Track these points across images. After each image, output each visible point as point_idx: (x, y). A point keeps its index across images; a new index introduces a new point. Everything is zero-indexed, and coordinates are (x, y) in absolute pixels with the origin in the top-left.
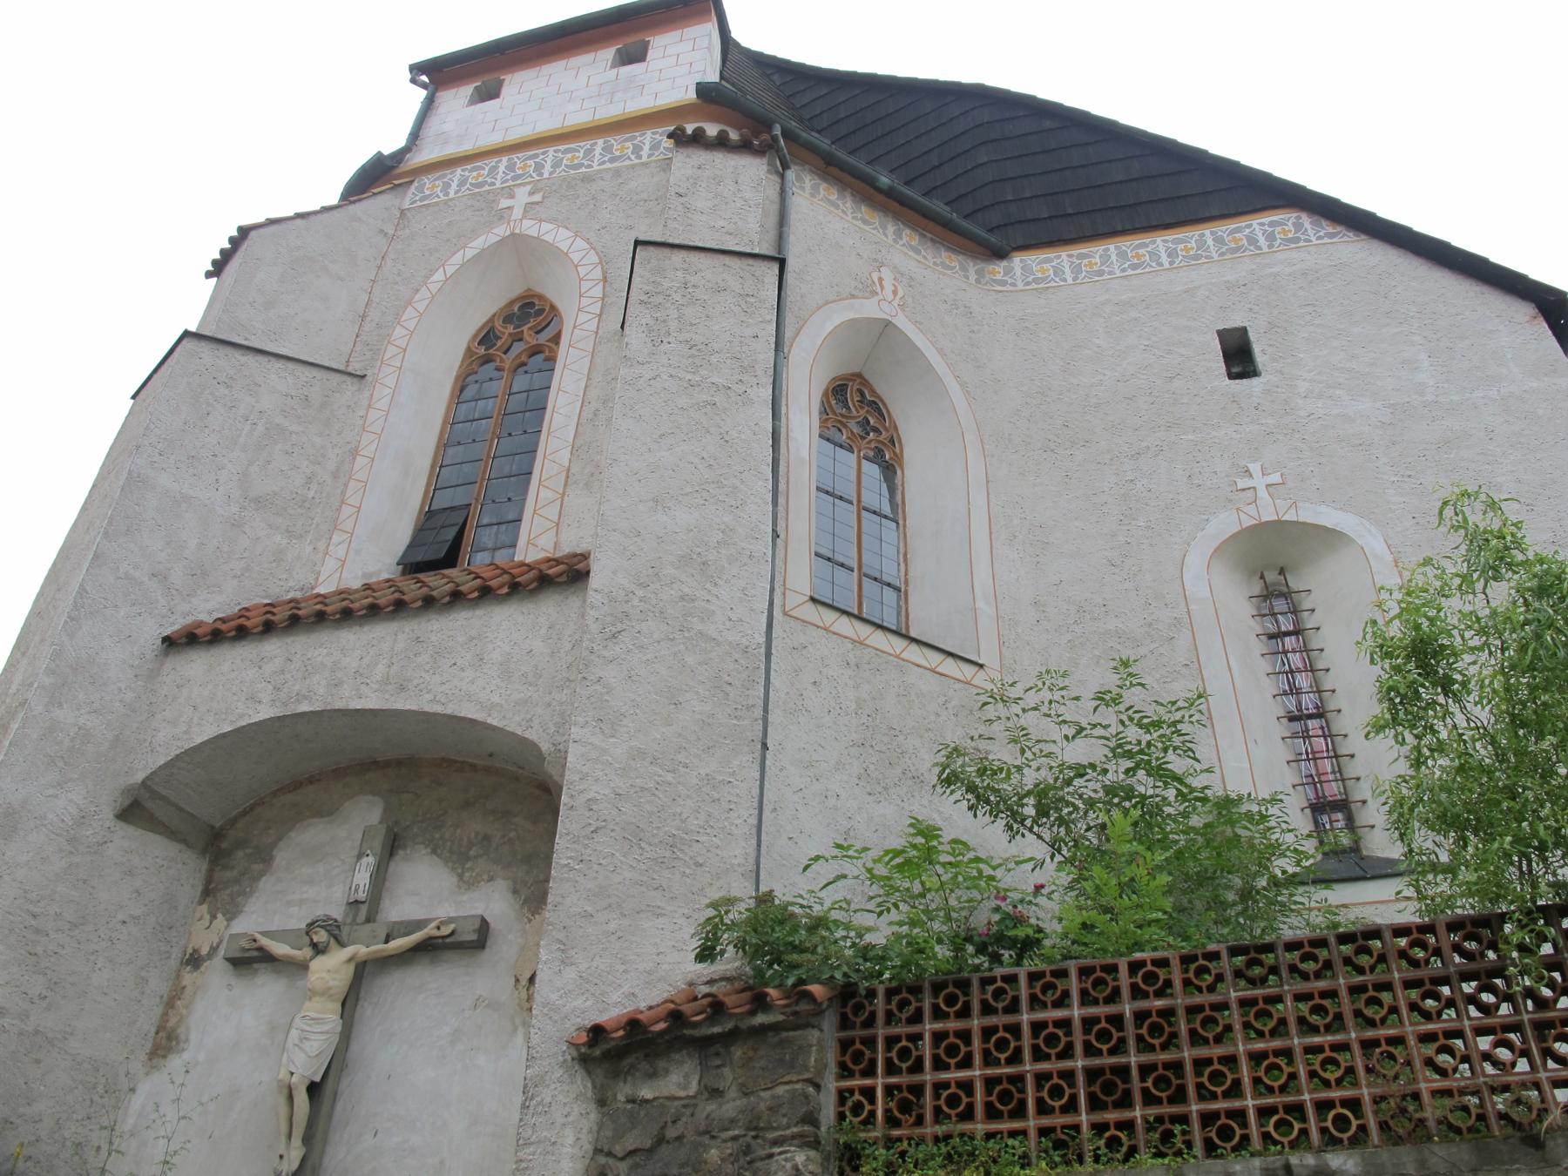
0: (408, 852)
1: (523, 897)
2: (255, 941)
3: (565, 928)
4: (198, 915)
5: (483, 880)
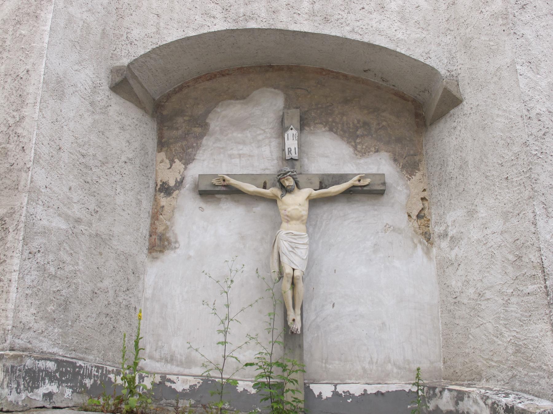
0: (312, 128)
1: (401, 164)
2: (224, 180)
3: (543, 194)
4: (159, 159)
5: (372, 151)
